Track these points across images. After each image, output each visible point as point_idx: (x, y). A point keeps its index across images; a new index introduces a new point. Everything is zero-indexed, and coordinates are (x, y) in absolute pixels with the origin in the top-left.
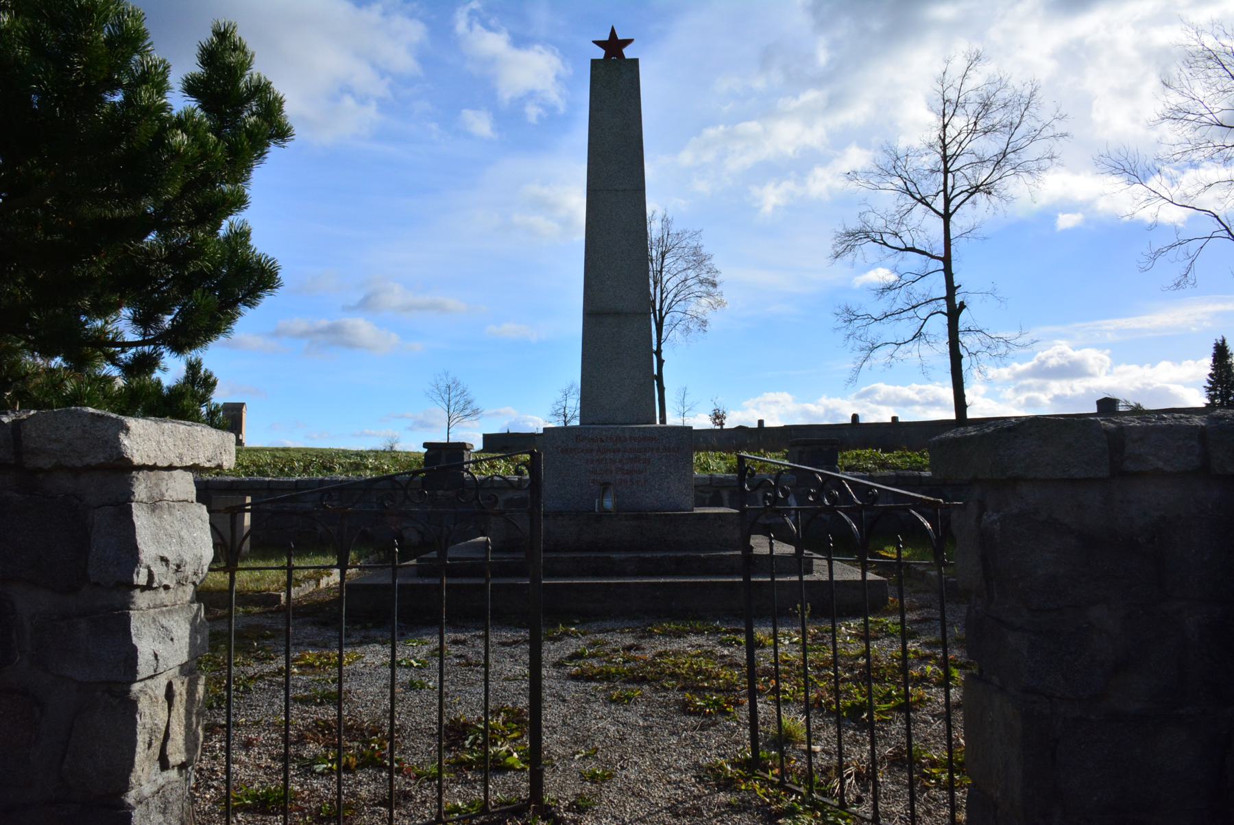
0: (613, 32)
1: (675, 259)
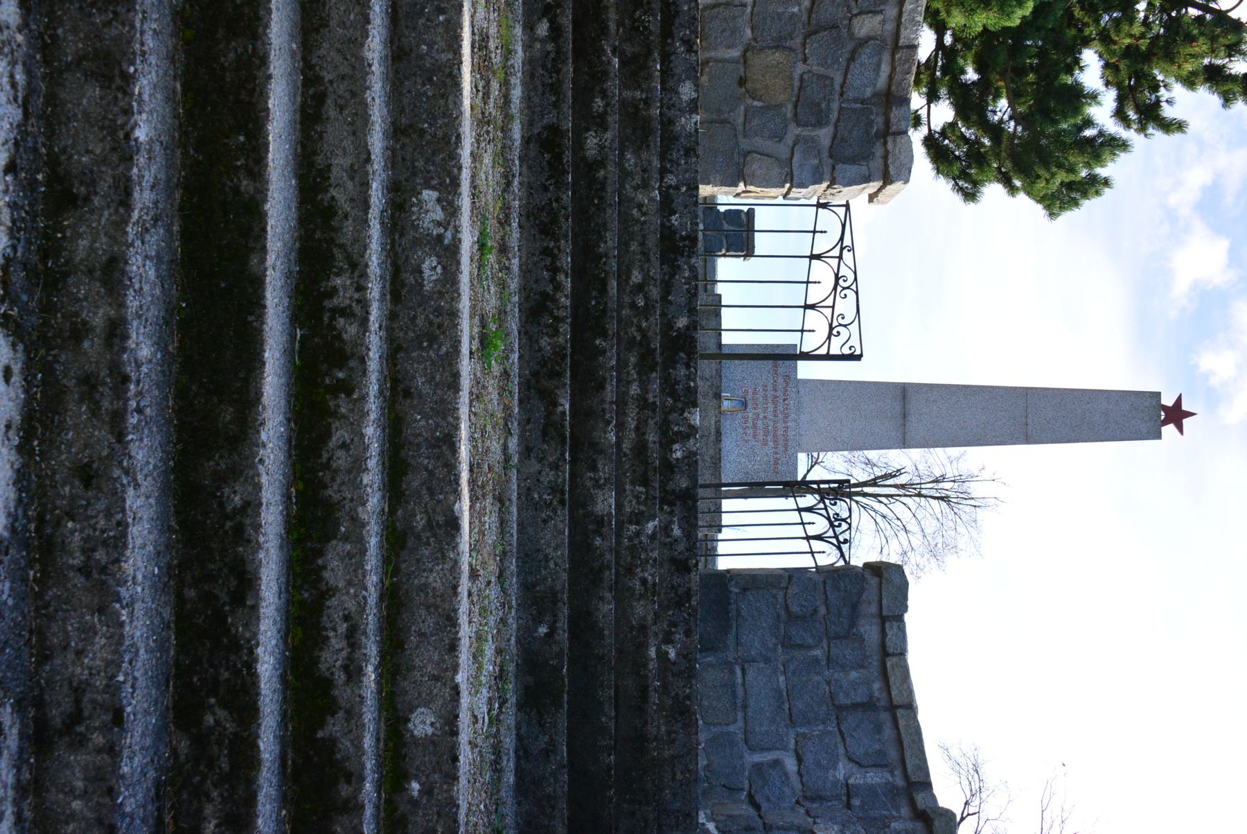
0: (1190, 414)
1: (939, 516)
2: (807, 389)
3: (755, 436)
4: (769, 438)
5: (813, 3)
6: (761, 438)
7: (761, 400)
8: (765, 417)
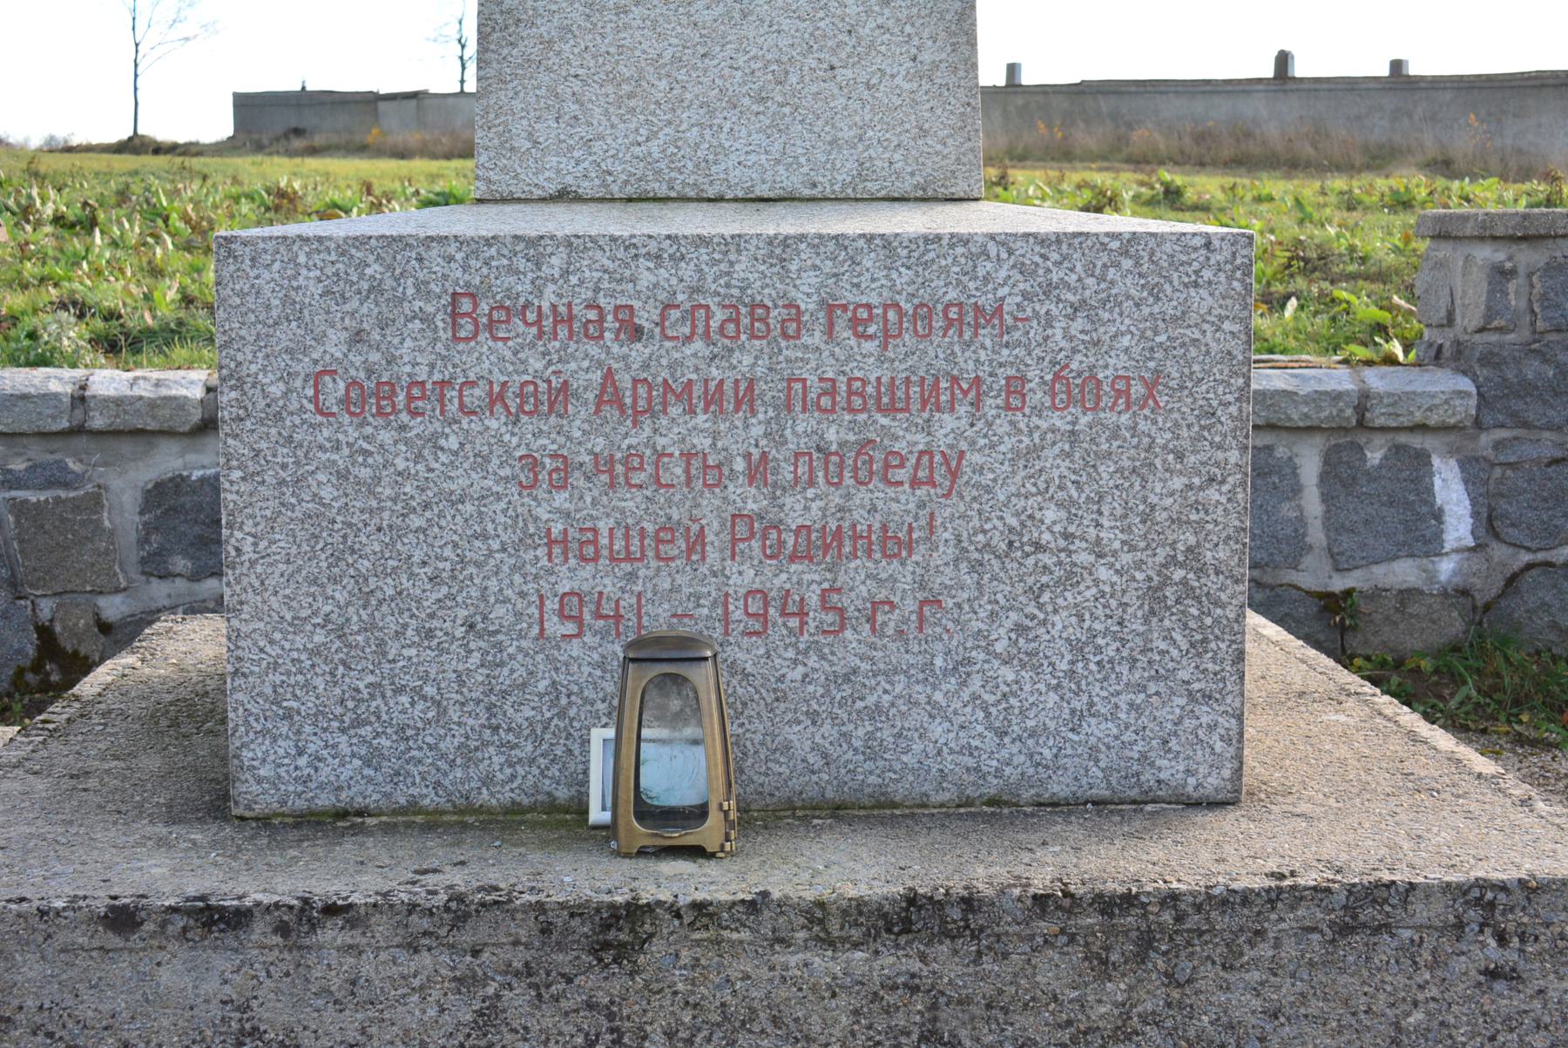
2: (547, 130)
3: (894, 544)
4: (908, 440)
5: (1564, 236)
6: (907, 499)
7: (631, 502)
8: (758, 470)
